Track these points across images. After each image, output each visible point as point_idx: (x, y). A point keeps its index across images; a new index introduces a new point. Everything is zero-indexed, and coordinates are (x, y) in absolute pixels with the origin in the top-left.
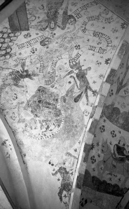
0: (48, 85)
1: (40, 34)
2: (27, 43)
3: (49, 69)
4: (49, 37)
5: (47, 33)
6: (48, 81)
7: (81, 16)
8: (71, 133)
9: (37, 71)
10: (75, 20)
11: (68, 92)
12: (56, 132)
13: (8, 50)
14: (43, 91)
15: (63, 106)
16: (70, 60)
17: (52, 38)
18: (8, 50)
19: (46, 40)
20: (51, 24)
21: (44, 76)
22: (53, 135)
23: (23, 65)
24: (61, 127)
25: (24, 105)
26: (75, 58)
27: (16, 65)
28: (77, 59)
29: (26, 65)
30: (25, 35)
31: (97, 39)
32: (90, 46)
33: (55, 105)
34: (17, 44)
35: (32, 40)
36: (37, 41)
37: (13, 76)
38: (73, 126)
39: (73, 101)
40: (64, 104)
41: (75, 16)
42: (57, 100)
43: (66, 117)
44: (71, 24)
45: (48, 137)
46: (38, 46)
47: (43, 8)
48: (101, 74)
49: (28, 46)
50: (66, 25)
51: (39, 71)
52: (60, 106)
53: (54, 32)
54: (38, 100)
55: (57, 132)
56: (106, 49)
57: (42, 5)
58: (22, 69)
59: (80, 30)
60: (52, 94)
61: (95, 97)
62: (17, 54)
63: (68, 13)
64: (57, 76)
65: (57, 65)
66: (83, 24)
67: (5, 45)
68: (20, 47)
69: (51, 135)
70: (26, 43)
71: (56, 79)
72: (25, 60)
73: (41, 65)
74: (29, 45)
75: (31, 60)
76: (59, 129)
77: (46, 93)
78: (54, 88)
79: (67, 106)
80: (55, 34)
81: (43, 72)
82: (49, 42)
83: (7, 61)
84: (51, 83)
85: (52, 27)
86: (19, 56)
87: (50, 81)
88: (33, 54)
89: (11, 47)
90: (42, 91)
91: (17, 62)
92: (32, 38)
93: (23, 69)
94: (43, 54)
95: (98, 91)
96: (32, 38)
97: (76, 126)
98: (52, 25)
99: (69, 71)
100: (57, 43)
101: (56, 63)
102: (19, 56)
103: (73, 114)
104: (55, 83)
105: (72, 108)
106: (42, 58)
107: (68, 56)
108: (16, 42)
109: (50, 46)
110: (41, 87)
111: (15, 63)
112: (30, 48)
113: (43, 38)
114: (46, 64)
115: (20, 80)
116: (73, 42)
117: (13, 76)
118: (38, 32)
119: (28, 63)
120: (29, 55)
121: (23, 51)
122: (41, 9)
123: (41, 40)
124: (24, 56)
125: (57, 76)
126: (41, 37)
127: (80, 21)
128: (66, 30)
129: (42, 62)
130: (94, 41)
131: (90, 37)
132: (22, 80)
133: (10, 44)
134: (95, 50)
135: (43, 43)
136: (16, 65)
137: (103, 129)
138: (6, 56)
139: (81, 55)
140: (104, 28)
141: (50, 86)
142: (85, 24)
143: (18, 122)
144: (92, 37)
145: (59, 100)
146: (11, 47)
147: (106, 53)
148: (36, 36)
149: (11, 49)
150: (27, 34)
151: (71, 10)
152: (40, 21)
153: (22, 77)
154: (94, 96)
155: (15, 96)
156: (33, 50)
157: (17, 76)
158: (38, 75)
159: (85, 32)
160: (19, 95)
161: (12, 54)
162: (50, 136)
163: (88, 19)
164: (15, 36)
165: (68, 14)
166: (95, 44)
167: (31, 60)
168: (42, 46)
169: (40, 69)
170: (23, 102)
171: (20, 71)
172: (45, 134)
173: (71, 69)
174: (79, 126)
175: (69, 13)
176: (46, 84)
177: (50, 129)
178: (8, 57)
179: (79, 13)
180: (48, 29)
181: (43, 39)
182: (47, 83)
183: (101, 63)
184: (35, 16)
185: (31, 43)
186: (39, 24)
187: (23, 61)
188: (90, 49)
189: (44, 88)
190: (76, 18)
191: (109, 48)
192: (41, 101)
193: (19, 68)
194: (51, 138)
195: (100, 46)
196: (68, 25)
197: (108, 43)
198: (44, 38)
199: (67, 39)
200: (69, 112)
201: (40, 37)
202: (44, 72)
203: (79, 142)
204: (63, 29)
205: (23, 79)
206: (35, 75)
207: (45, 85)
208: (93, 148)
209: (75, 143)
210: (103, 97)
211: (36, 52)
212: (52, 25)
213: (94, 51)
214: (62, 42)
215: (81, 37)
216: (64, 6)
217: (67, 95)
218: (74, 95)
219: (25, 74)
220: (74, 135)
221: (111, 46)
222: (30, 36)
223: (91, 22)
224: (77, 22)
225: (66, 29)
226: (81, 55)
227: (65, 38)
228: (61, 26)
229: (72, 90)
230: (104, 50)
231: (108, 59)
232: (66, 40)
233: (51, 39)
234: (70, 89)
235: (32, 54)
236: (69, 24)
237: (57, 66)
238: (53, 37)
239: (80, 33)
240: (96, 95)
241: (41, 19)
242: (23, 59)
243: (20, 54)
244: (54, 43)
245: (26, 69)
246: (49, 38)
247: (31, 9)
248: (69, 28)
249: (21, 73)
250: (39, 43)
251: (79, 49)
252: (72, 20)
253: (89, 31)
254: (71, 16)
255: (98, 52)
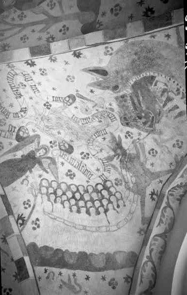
0: (114, 116)
1: (61, 160)
2: (80, 169)
3: (96, 123)
4: (58, 147)
5: (55, 152)
6: (110, 118)
7: (11, 126)
8: (149, 55)
9: (108, 137)
10: (19, 130)
11: (104, 88)
12: (164, 76)
13: (100, 187)
14: (125, 118)
15: (125, 86)
16: (69, 105)
17: (57, 143)
18: (100, 187)
19: (63, 147)
20: (41, 155)
21: (108, 125)
22: (170, 79)
23: (110, 159)
24: (152, 74)
25: (156, 136)
26: (60, 101)
27: (114, 167)
28: (61, 98)
29: (108, 155)
30: (70, 178)
31: (21, 91)
32: (35, 92)
33: (130, 97)
34: (88, 182)
35: (73, 165)
36: (71, 158)
37: (129, 166)
38: (139, 59)
39: (108, 76)
40: (120, 86)
41: (15, 134)
42: (123, 97)
43: (135, 74)
44: (27, 131)
45: (178, 84)
46: (76, 154)
47: (26, 179)
48: (51, 61)
49: (83, 166)
50: (32, 137)
51: (106, 135)
52: (127, 90)
53: (49, 145)
54: (139, 120)
55: (162, 75)
56: (21, 74)
57: (22, 183)
58: (115, 158)
59: (27, 116)
60: (122, 106)
61: (82, 52)
62: (100, 174)
63: (16, 144)
64: (97, 110)
65: (85, 116)
66: (18, 117)
67: (95, 196)
68: (90, 174)
69: (172, 82)
70: (81, 171)
71: (101, 110)
72: (102, 161)
73: (98, 136)
74: (82, 165)
75: (98, 153)
76: (156, 75)
77: (125, 114)
78: (111, 107)
79: (120, 81)
80: (51, 142)
81: (105, 129)
82: (64, 144)
83: (114, 182)
84: (110, 113)
85: (44, 151)
86: (101, 170)
87: (108, 116)
88: (90, 154)
89: (94, 186)
90: (126, 120)
91: (110, 169)
92: (70, 167)
93: (115, 156)
94: (83, 142)
95: (72, 52)
96: (70, 167)
97: (136, 54)
98: (42, 152)
99: (80, 99)
100: (59, 133)
101: (83, 119)
102: (101, 170)
103: (124, 67)
104: (106, 108)
105: (117, 72)
106: (89, 140)
107: (66, 110)
108: (86, 184)
109: (67, 139)
110: (122, 124)
111: (112, 170)
112: (85, 161)
113: (63, 154)
114: (93, 131)
115: (130, 154)
116: (46, 114)
117: (129, 166)
118: (59, 165)
119: (104, 155)
120: (93, 158)
121: (93, 169)
122: (28, 181)
123: (68, 155)
124: (98, 164)
125: (97, 110)
126: (63, 157)
127: (16, 123)
128: (38, 132)
129: (94, 137)
130: (26, 92)
131: (27, 100)
132: (128, 152)
133: (90, 190)
134: (34, 84)
135: (70, 150)
136: (114, 167)
137: (115, 9)
138: (109, 186)
139: (53, 97)
140: (4, 90)
141: (114, 113)
142: (16, 115)
143: (182, 135)
144: (24, 96)
145: (121, 94)
146: (94, 186)
147: (24, 71)
148: (66, 164)
149: (97, 184)
150: (69, 177)
151: (11, 144)
152: (44, 172)
153: (124, 153)
154: (81, 54)
155: (151, 152)
156: (85, 156)
157: (126, 160)
158: (111, 134)
159: (26, 108)
160: (147, 148)
161: (103, 181)
162: (174, 82)
163: (8, 116)
164: (78, 189)
165: (17, 143)
166: (28, 88)
167: (98, 153)
168: (73, 149)
169: (103, 135)
170: (153, 138)
171: (119, 159)
172: (176, 91)
173: (77, 98)
174: (132, 49)
175: (15, 143)
176: (115, 119)
177: (166, 87)
178: (108, 184)
179: (8, 131)
180: (50, 155)
181: (65, 153)
182: (113, 119)
183: (40, 70)
184: (41, 183)
185: (78, 164)
186: (49, 170)
187: (106, 161)
188: (38, 90)
189: (121, 118)
190: (16, 130)
191: (18, 72)
192: (138, 117)
193: (116, 162)
194: (176, 80)
195: (25, 83)
196: (31, 134)
197: (14, 75)
198: (62, 152)
199: (46, 124)
200: (125, 73)
201: (64, 159)
202: (103, 128)
203: (152, 38)
204: (38, 136)
205: (126, 151)
206: (113, 138)
207: (116, 120)
208: (150, 7)
209: (159, 43)
210: (71, 43)
211: (86, 151)
212: (42, 152)
213: (35, 86)
214: (55, 128)
215: (35, 109)
216: (10, 157)
217: (108, 88)
218: (101, 79)
219: (119, 151)
220: (150, 51)
221: (13, 70)
222: (69, 171)
223: (10, 110)
224: (21, 126)
225: (36, 133)
226: (53, 97)
227: (48, 127)
228: (36, 141)
229: (99, 84)
230: (24, 75)
231: (28, 65)
232: (49, 125)
233: (59, 144)
234: (99, 87)
235: (90, 156)
236: (28, 133)
237: (87, 116)
238: (55, 142)
239: (31, 112)
240: (78, 51)
241: (41, 172)
242: (103, 163)
243: (98, 170)
244: (62, 136)
245: (112, 153)
246: (59, 146)
247: (33, 194)
248: (34, 131)
249: (120, 157)
250: (72, 154)
251: (48, 103)
252: (21, 133)
253: (21, 104)
254: (18, 138)
255: (32, 80)
